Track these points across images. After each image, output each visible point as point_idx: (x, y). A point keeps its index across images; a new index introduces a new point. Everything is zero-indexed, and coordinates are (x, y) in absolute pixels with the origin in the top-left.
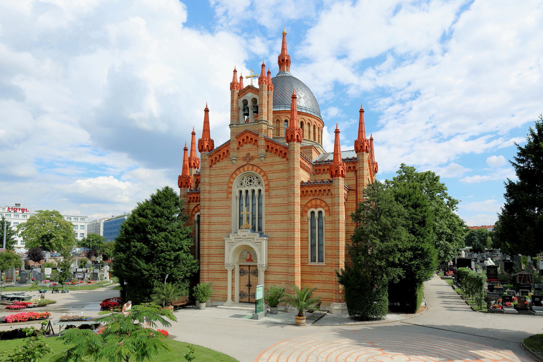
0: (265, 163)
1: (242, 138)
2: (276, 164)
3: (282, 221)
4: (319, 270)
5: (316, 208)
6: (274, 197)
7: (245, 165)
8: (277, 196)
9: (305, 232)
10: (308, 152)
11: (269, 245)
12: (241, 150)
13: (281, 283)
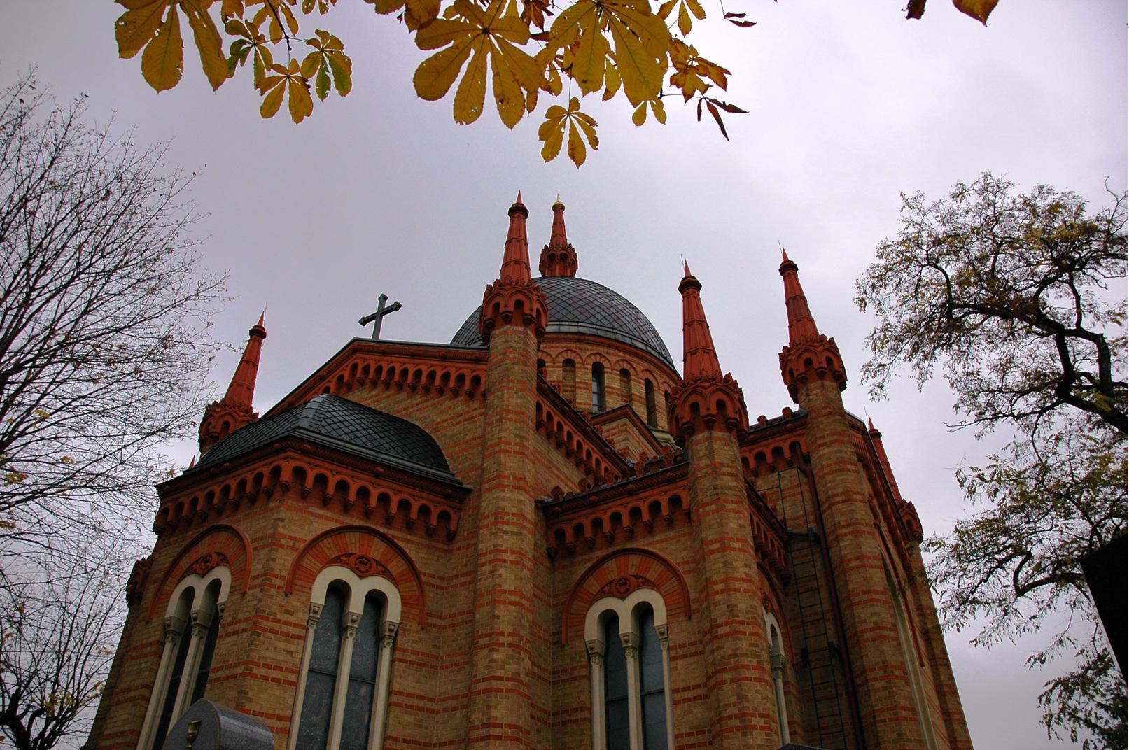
5: (623, 596)
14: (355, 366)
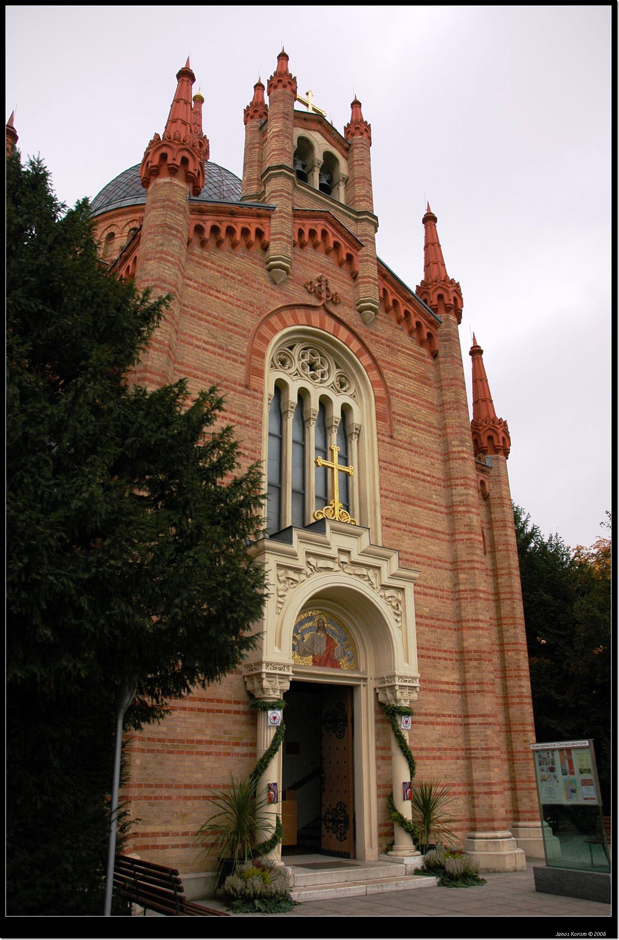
3: (432, 530)
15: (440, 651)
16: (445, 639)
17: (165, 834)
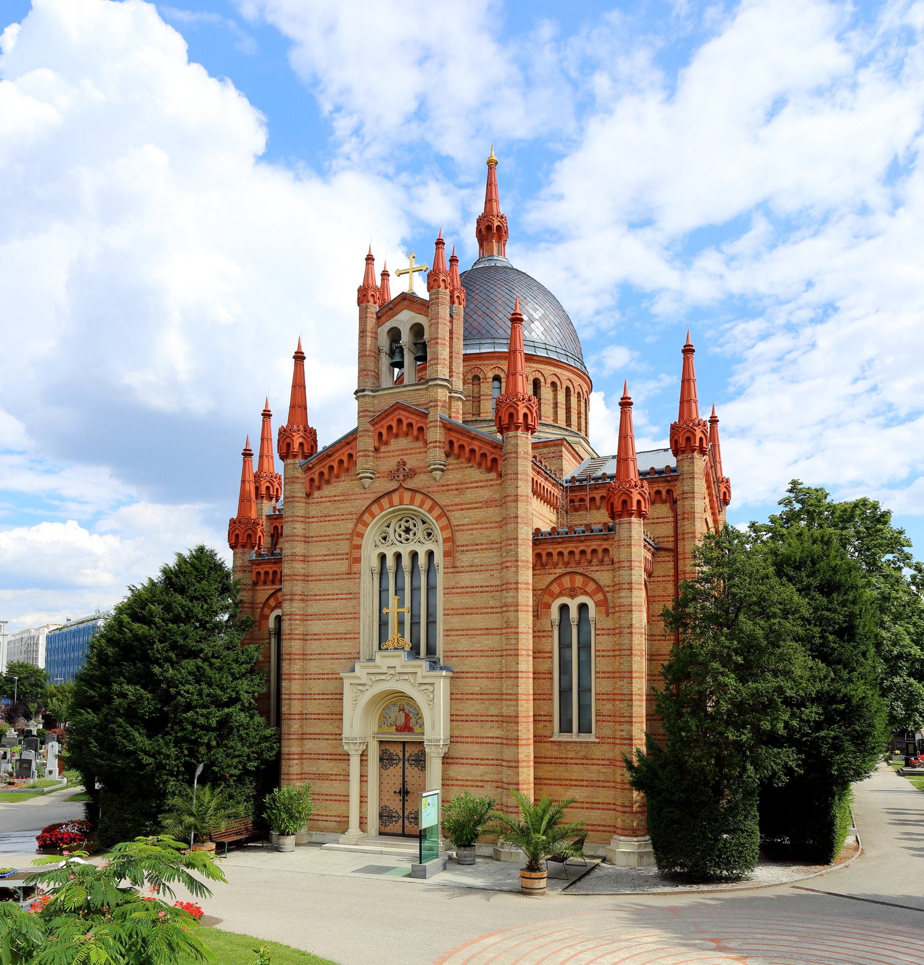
0: (443, 486)
1: (386, 423)
2: (472, 488)
4: (582, 754)
6: (467, 569)
7: (394, 491)
8: (474, 568)
9: (544, 658)
10: (553, 455)
11: (454, 691)
12: (384, 452)
13: (483, 787)
14: (400, 421)
15: (488, 716)
16: (493, 707)
17: (318, 815)
